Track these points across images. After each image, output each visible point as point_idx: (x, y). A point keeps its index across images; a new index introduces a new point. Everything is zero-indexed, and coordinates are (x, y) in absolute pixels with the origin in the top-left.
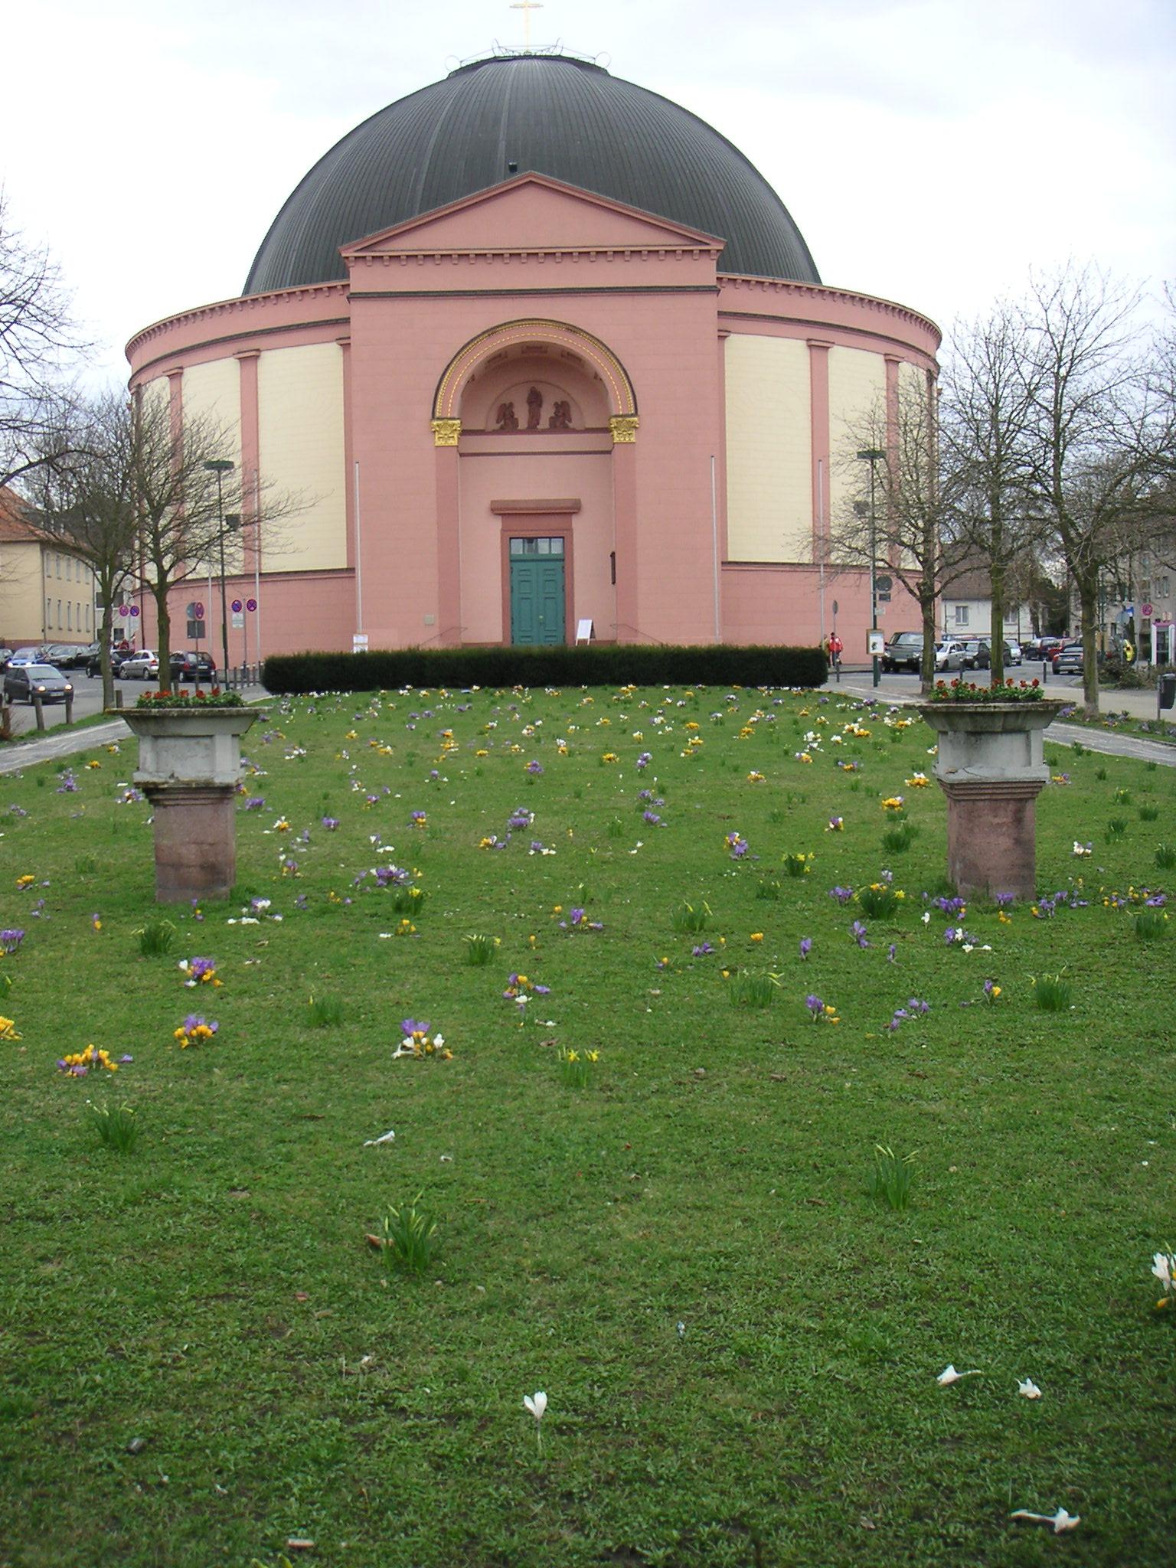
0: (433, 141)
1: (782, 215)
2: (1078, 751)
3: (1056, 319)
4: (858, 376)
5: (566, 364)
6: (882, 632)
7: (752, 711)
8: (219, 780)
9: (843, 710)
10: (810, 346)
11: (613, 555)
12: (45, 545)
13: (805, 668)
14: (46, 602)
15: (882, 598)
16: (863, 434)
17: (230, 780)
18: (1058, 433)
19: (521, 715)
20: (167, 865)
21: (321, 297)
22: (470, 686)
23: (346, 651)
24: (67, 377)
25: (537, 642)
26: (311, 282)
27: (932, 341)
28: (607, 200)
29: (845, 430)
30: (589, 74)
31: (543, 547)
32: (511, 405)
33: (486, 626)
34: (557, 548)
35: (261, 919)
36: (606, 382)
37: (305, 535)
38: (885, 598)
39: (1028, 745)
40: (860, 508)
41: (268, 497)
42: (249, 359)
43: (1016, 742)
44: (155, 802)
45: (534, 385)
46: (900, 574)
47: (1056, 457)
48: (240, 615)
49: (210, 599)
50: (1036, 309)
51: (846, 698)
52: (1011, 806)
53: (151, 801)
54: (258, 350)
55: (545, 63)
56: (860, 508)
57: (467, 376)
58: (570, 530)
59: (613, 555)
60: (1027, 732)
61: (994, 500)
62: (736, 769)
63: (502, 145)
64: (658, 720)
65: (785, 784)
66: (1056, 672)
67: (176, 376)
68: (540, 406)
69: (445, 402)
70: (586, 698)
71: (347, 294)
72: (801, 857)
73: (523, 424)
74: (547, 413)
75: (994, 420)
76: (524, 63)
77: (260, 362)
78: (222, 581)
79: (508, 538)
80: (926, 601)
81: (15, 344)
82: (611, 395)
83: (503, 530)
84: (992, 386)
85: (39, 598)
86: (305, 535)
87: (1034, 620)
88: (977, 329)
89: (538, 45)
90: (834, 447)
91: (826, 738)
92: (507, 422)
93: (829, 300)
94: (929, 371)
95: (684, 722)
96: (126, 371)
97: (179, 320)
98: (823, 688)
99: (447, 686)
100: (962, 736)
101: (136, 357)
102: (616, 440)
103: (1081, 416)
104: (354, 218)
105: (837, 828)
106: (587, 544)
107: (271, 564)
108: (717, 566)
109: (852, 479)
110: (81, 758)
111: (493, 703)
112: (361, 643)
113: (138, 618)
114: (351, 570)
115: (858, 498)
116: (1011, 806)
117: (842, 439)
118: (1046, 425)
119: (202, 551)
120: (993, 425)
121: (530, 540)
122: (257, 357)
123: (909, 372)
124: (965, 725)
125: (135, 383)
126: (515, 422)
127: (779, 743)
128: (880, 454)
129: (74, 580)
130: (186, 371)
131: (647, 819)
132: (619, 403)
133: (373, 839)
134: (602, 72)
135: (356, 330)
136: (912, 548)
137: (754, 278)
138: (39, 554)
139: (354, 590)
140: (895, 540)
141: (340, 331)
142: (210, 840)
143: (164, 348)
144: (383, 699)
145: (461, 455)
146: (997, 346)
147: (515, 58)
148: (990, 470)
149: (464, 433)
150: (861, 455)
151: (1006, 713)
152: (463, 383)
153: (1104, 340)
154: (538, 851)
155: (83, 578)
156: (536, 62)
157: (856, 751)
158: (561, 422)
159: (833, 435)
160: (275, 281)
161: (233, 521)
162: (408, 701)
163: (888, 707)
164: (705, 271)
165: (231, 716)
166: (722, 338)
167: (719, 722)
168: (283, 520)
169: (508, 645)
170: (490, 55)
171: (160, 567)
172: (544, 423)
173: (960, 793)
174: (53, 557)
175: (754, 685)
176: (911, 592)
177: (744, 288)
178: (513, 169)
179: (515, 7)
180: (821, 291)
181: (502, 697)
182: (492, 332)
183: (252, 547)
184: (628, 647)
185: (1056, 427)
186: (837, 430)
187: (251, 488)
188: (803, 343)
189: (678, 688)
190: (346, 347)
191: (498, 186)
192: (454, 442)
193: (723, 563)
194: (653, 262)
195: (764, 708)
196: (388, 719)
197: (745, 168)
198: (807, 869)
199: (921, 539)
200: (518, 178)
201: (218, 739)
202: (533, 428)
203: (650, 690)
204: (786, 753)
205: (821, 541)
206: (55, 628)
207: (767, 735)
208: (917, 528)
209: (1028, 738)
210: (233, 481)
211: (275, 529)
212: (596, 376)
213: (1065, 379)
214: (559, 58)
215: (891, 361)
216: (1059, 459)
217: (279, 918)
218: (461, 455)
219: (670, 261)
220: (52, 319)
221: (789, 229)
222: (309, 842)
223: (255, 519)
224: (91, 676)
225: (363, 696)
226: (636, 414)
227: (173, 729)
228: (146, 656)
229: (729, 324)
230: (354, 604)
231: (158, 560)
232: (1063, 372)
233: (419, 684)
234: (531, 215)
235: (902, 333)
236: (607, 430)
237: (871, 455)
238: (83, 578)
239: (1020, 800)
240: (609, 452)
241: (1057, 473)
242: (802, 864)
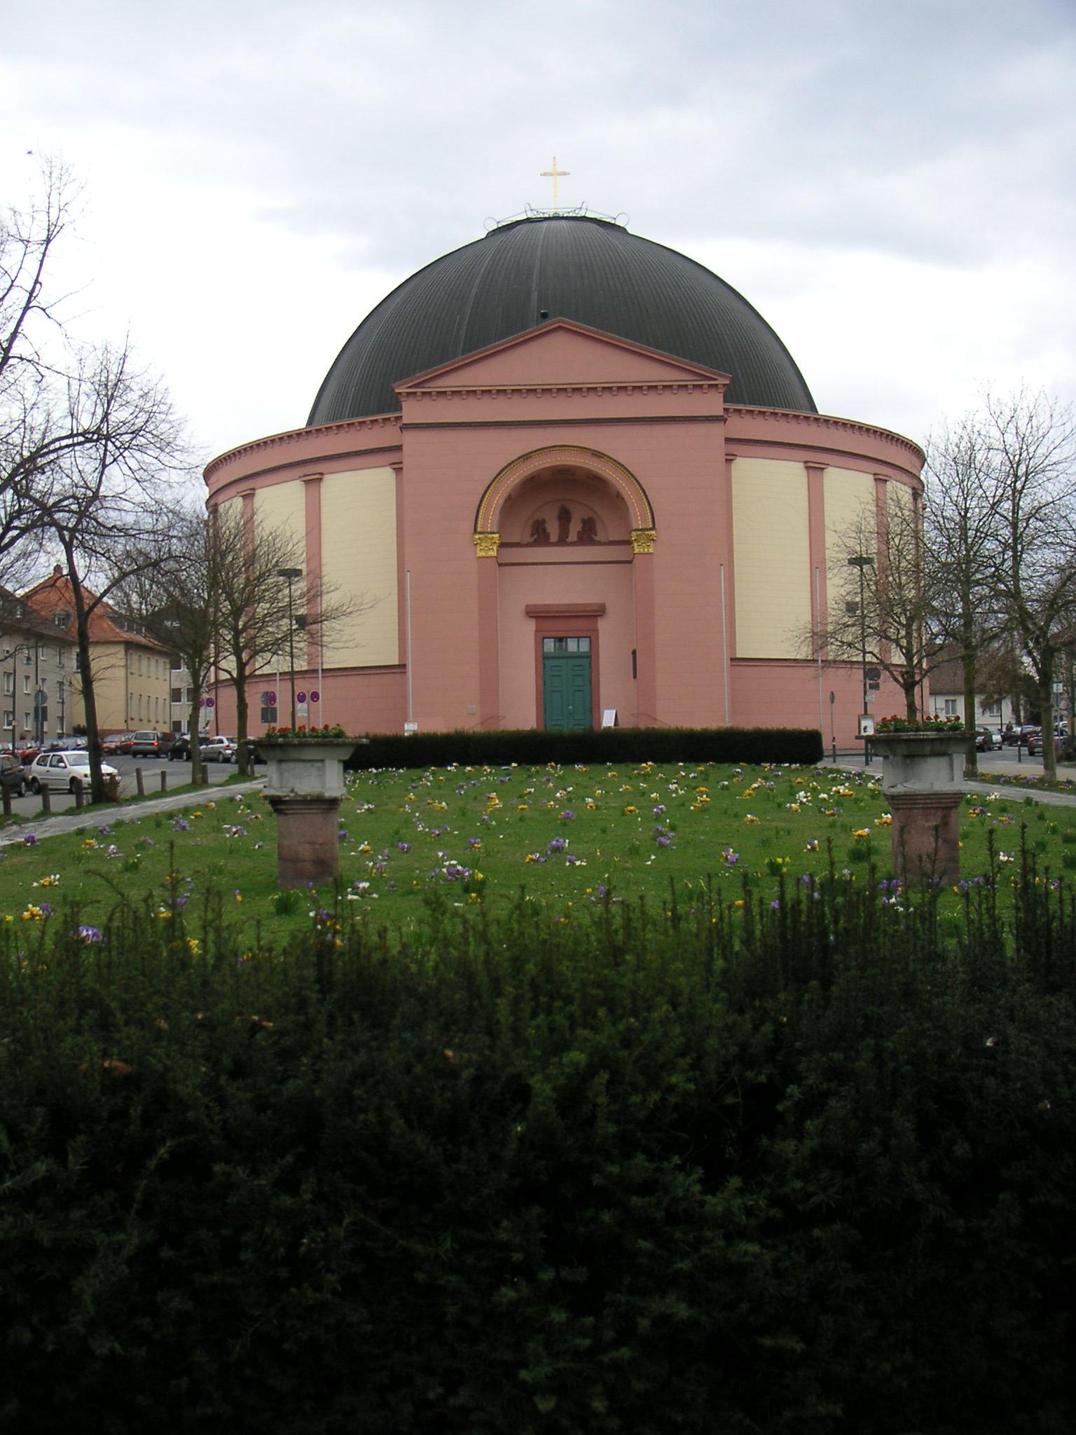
0: (474, 291)
1: (781, 352)
2: (1028, 802)
3: (1010, 438)
4: (849, 492)
5: (593, 485)
6: (871, 717)
7: (754, 782)
8: (328, 795)
9: (834, 779)
10: (807, 468)
11: (634, 652)
12: (130, 646)
13: (801, 748)
14: (129, 697)
15: (872, 687)
16: (851, 543)
17: (336, 793)
18: (1017, 538)
19: (555, 786)
20: (287, 860)
21: (376, 428)
22: (509, 764)
23: (400, 733)
24: (177, 492)
25: (568, 725)
26: (367, 415)
27: (917, 462)
28: (627, 342)
29: (837, 540)
30: (610, 232)
31: (572, 646)
32: (543, 521)
33: (522, 716)
34: (584, 646)
35: (362, 896)
36: (629, 503)
37: (362, 635)
38: (875, 687)
39: (951, 765)
40: (851, 607)
41: (329, 601)
42: (313, 482)
43: (942, 763)
44: (279, 812)
45: (564, 503)
46: (887, 667)
47: (1014, 557)
48: (305, 705)
49: (282, 691)
50: (995, 433)
51: (838, 771)
52: (940, 813)
53: (276, 811)
54: (322, 474)
55: (572, 223)
56: (851, 607)
57: (505, 495)
58: (596, 630)
59: (634, 652)
60: (950, 755)
61: (964, 598)
62: (736, 816)
63: (535, 295)
64: (673, 787)
65: (774, 824)
66: (1032, 754)
67: (249, 496)
68: (569, 521)
69: (486, 519)
70: (611, 772)
71: (400, 424)
72: (780, 860)
73: (554, 538)
74: (575, 528)
75: (964, 529)
76: (554, 223)
77: (323, 484)
78: (292, 675)
80: (909, 687)
81: (134, 465)
82: (631, 511)
83: (537, 631)
84: (961, 499)
85: (123, 692)
86: (362, 635)
87: (1016, 711)
88: (946, 450)
89: (565, 207)
90: (830, 553)
91: (815, 797)
92: (540, 536)
93: (824, 427)
94: (913, 489)
95: (695, 788)
96: (205, 493)
97: (251, 447)
98: (820, 765)
99: (489, 764)
100: (899, 759)
101: (213, 479)
102: (637, 551)
103: (1033, 523)
104: (409, 357)
105: (813, 849)
106: (611, 642)
107: (333, 658)
108: (726, 663)
109: (842, 582)
110: (186, 811)
111: (530, 776)
112: (410, 728)
113: (213, 709)
114: (402, 666)
115: (849, 598)
116: (940, 813)
117: (836, 548)
118: (1006, 533)
119: (275, 646)
120: (962, 531)
121: (560, 640)
122: (320, 480)
123: (900, 491)
124: (902, 749)
125: (213, 502)
126: (547, 536)
127: (772, 801)
128: (869, 561)
129: (153, 677)
130: (258, 492)
131: (660, 843)
132: (638, 518)
133: (441, 854)
134: (622, 230)
136: (897, 642)
138: (123, 652)
139: (405, 684)
140: (883, 635)
141: (394, 457)
142: (321, 840)
143: (239, 471)
144: (433, 773)
145: (500, 565)
146: (966, 464)
147: (546, 219)
148: (962, 573)
149: (502, 545)
150: (852, 562)
151: (933, 740)
152: (501, 501)
153: (1053, 458)
154: (572, 862)
155: (161, 676)
156: (563, 223)
157: (838, 804)
158: (588, 536)
159: (828, 545)
160: (335, 414)
161: (302, 622)
162: (456, 775)
163: (873, 777)
164: (713, 403)
165: (338, 745)
166: (729, 461)
167: (724, 787)
168: (345, 620)
169: (542, 728)
170: (523, 217)
171: (239, 658)
172: (573, 536)
173: (899, 803)
174: (135, 657)
175: (758, 763)
176: (896, 680)
177: (748, 418)
178: (544, 316)
179: (545, 174)
180: (817, 420)
181: (537, 772)
182: (526, 457)
183: (316, 641)
184: (647, 729)
185: (1014, 534)
186: (830, 539)
187: (314, 594)
188: (801, 465)
189: (692, 766)
190: (398, 471)
191: (532, 330)
192: (493, 553)
193: (732, 659)
195: (766, 779)
196: (439, 788)
197: (748, 311)
198: (785, 870)
199: (903, 633)
200: (549, 324)
201: (328, 763)
202: (562, 541)
203: (666, 766)
204: (779, 805)
205: (819, 637)
206: (137, 720)
207: (765, 796)
208: (899, 623)
209: (951, 761)
210: (300, 586)
211: (339, 627)
212: (619, 496)
213: (1021, 492)
214: (584, 219)
215: (880, 480)
216: (1017, 560)
217: (375, 896)
218: (500, 565)
219: (683, 395)
220: (165, 445)
221: (787, 364)
222: (389, 859)
223: (319, 619)
224: (171, 760)
225: (415, 773)
226: (654, 528)
227: (295, 754)
228: (221, 742)
229: (734, 448)
230: (405, 697)
231: (238, 653)
232: (1019, 485)
233: (464, 763)
234: (556, 352)
235: (889, 455)
236: (629, 543)
237: (858, 561)
238: (161, 676)
239: (946, 808)
240: (630, 562)
241: (1016, 572)
242: (779, 867)
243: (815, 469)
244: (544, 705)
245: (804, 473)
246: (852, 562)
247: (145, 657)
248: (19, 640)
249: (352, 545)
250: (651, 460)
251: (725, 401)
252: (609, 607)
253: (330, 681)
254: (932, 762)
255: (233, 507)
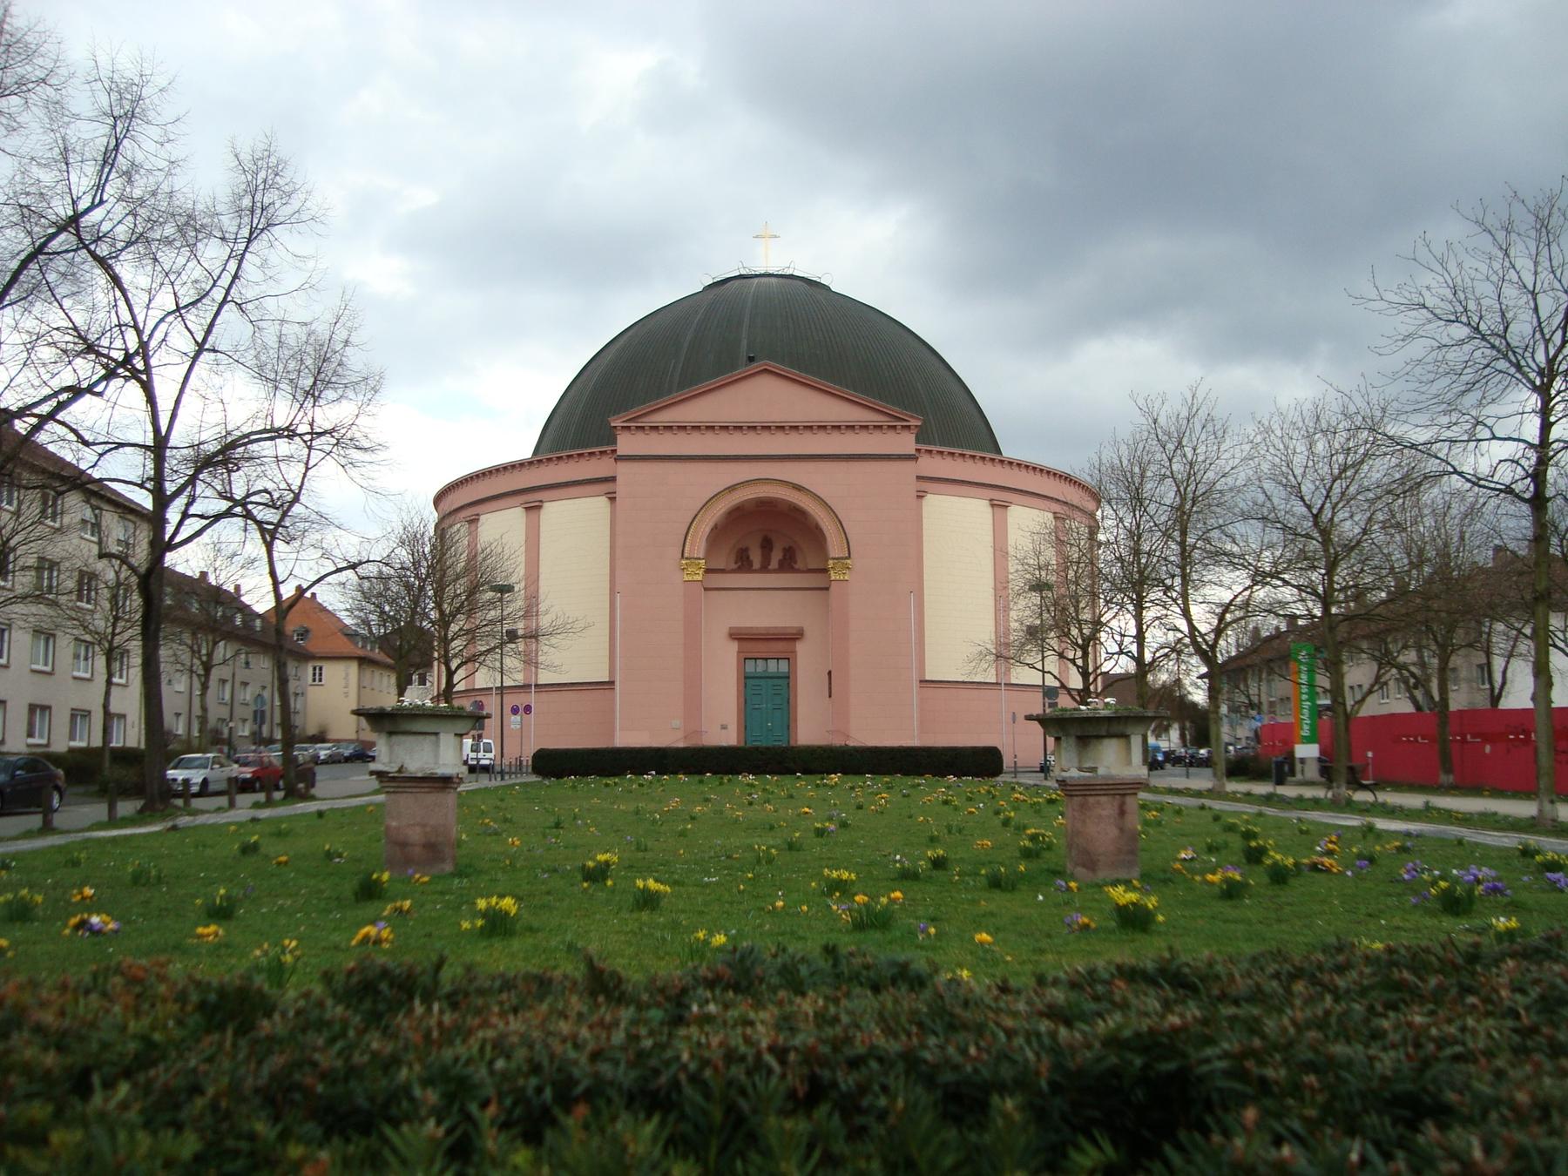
7: (932, 791)
10: (993, 506)
12: (363, 661)
13: (984, 762)
26: (587, 447)
33: (722, 729)
42: (533, 508)
45: (770, 537)
48: (518, 718)
57: (711, 524)
58: (794, 652)
67: (474, 521)
73: (756, 565)
74: (776, 556)
79: (744, 659)
86: (574, 656)
87: (1182, 736)
92: (743, 563)
100: (1072, 741)
101: (441, 506)
106: (808, 664)
108: (915, 684)
114: (612, 683)
122: (539, 507)
126: (750, 563)
128: (1049, 587)
132: (835, 548)
134: (827, 288)
135: (620, 487)
136: (1073, 661)
137: (957, 451)
139: (614, 700)
149: (708, 571)
152: (708, 529)
156: (773, 280)
164: (905, 442)
172: (774, 564)
177: (938, 458)
178: (751, 359)
180: (1002, 462)
182: (732, 489)
186: (1013, 566)
187: (530, 611)
190: (612, 500)
191: (738, 373)
194: (864, 435)
201: (442, 736)
202: (764, 568)
212: (818, 528)
214: (792, 277)
223: (533, 636)
230: (613, 711)
237: (1039, 587)
243: (998, 506)
244: (745, 726)
245: (989, 509)
246: (1033, 588)
247: (377, 673)
248: (236, 646)
249: (571, 569)
250: (844, 494)
251: (917, 441)
252: (807, 633)
253: (544, 696)
254: (1106, 742)
255: (459, 529)
